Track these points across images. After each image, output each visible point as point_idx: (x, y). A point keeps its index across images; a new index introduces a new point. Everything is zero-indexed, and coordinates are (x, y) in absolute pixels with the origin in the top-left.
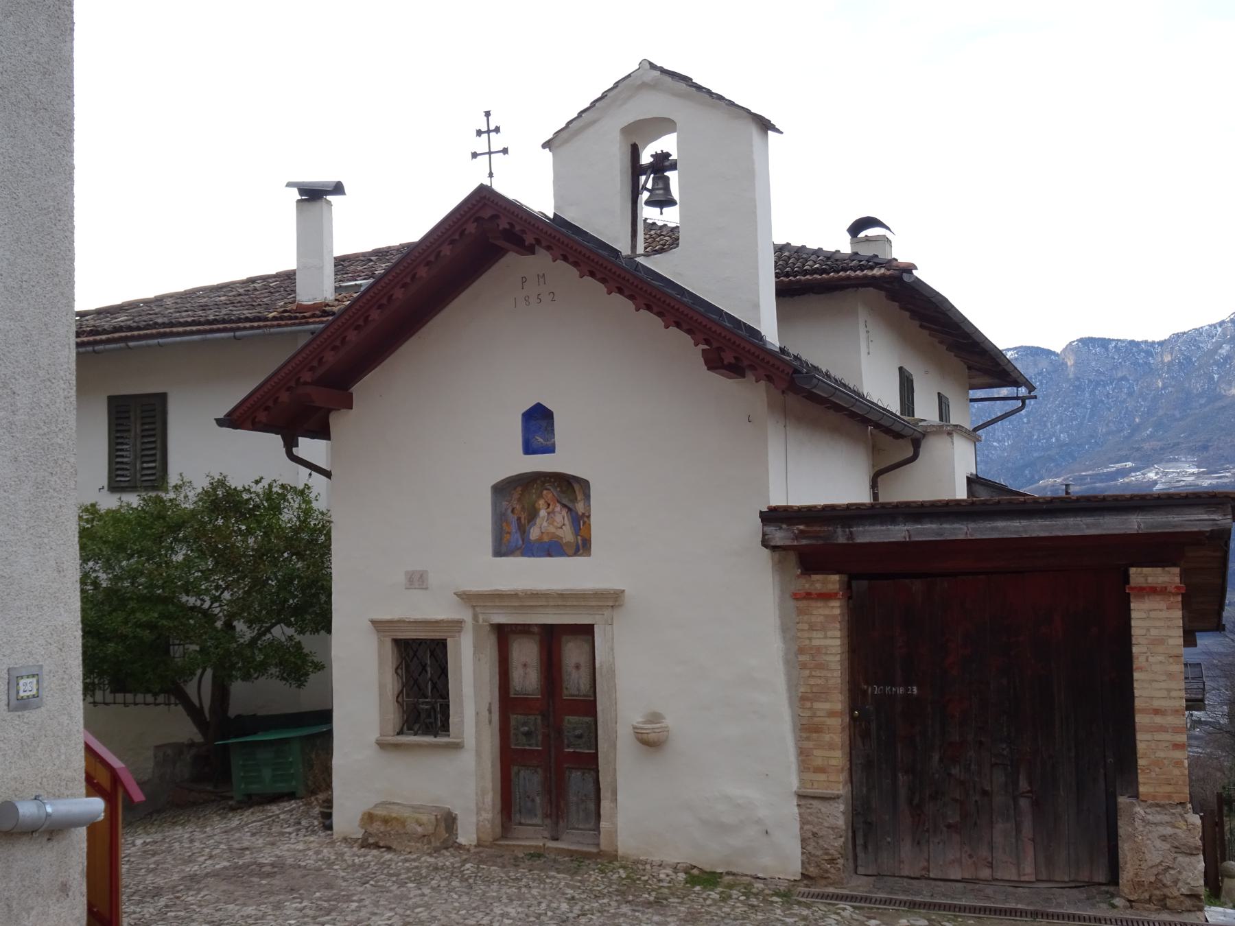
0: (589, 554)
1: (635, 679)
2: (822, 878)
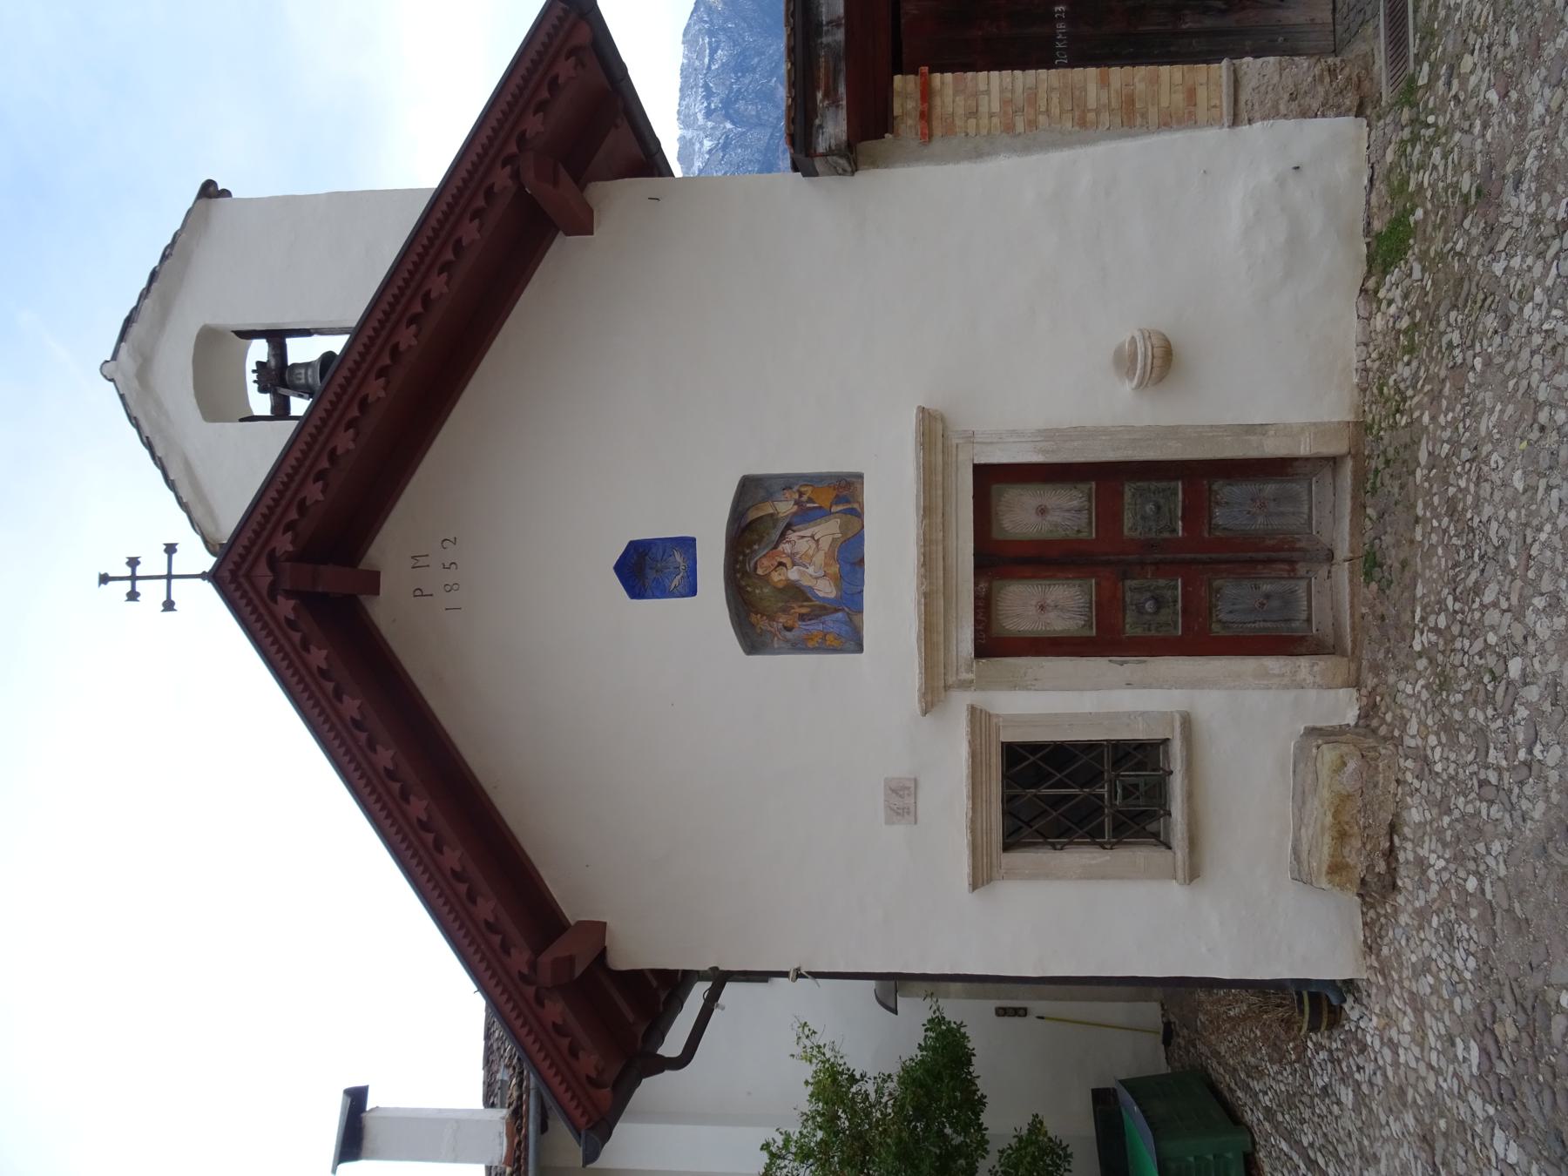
0: (860, 476)
1: (1062, 397)
2: (1359, 87)
